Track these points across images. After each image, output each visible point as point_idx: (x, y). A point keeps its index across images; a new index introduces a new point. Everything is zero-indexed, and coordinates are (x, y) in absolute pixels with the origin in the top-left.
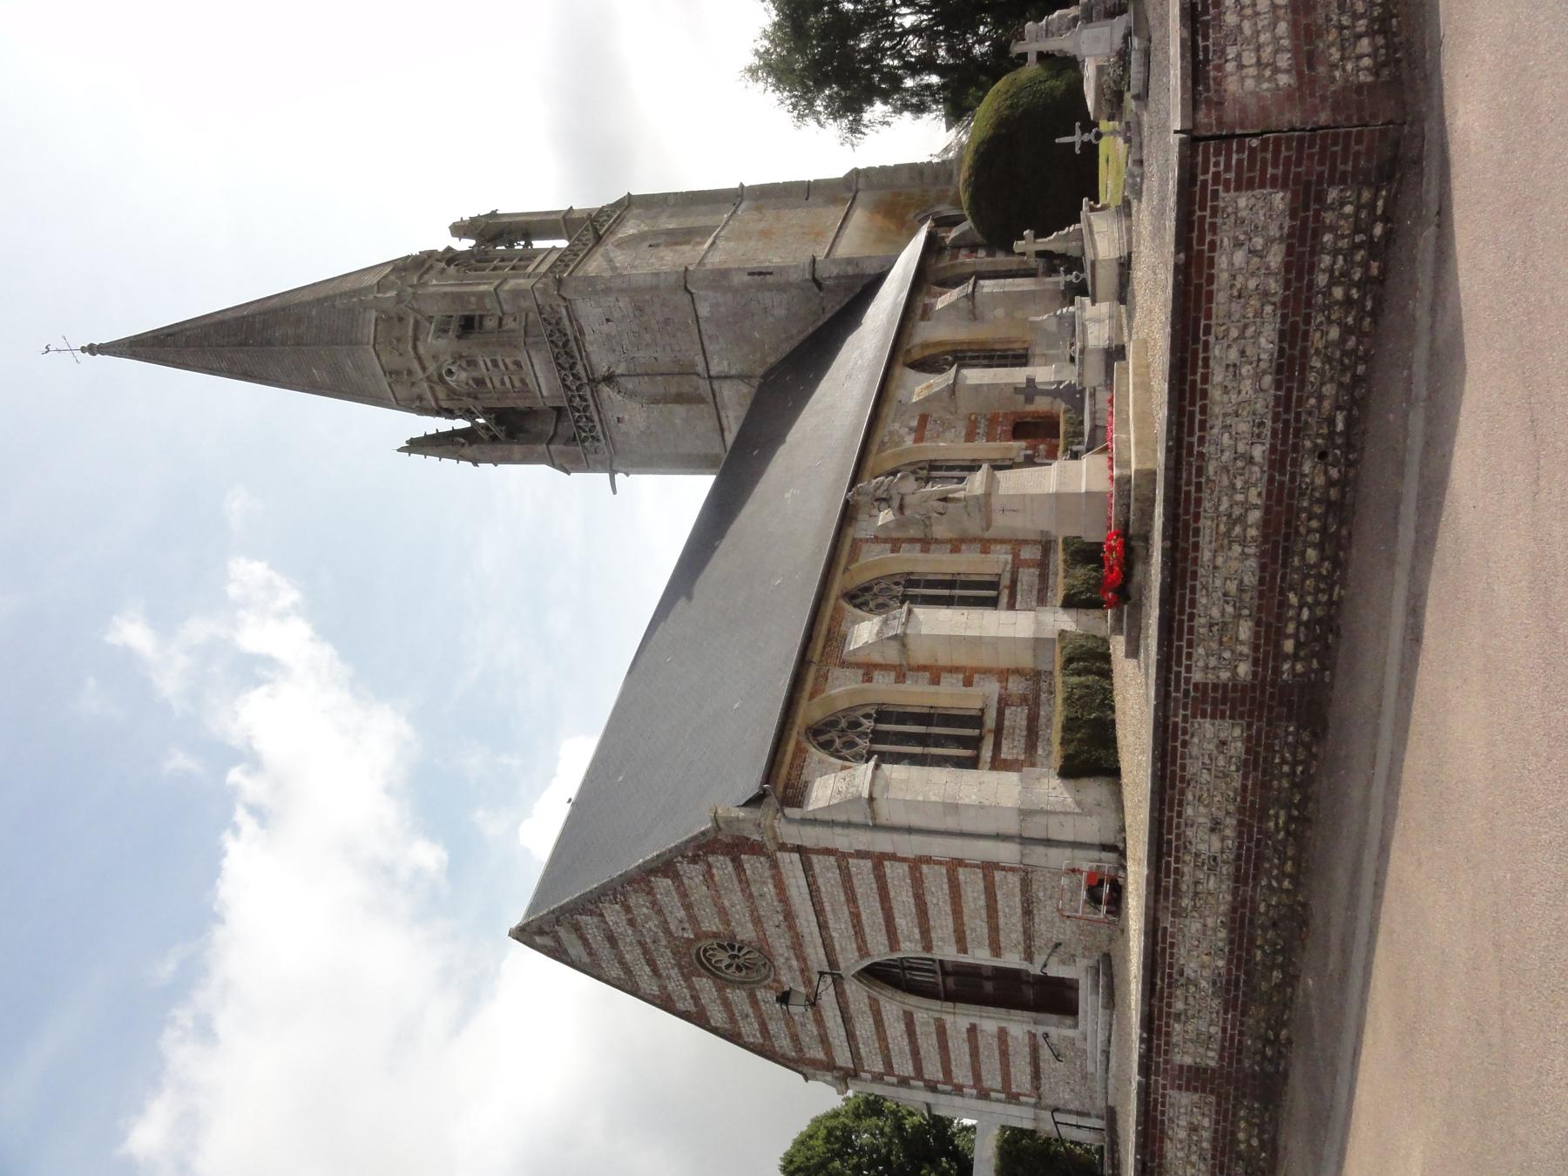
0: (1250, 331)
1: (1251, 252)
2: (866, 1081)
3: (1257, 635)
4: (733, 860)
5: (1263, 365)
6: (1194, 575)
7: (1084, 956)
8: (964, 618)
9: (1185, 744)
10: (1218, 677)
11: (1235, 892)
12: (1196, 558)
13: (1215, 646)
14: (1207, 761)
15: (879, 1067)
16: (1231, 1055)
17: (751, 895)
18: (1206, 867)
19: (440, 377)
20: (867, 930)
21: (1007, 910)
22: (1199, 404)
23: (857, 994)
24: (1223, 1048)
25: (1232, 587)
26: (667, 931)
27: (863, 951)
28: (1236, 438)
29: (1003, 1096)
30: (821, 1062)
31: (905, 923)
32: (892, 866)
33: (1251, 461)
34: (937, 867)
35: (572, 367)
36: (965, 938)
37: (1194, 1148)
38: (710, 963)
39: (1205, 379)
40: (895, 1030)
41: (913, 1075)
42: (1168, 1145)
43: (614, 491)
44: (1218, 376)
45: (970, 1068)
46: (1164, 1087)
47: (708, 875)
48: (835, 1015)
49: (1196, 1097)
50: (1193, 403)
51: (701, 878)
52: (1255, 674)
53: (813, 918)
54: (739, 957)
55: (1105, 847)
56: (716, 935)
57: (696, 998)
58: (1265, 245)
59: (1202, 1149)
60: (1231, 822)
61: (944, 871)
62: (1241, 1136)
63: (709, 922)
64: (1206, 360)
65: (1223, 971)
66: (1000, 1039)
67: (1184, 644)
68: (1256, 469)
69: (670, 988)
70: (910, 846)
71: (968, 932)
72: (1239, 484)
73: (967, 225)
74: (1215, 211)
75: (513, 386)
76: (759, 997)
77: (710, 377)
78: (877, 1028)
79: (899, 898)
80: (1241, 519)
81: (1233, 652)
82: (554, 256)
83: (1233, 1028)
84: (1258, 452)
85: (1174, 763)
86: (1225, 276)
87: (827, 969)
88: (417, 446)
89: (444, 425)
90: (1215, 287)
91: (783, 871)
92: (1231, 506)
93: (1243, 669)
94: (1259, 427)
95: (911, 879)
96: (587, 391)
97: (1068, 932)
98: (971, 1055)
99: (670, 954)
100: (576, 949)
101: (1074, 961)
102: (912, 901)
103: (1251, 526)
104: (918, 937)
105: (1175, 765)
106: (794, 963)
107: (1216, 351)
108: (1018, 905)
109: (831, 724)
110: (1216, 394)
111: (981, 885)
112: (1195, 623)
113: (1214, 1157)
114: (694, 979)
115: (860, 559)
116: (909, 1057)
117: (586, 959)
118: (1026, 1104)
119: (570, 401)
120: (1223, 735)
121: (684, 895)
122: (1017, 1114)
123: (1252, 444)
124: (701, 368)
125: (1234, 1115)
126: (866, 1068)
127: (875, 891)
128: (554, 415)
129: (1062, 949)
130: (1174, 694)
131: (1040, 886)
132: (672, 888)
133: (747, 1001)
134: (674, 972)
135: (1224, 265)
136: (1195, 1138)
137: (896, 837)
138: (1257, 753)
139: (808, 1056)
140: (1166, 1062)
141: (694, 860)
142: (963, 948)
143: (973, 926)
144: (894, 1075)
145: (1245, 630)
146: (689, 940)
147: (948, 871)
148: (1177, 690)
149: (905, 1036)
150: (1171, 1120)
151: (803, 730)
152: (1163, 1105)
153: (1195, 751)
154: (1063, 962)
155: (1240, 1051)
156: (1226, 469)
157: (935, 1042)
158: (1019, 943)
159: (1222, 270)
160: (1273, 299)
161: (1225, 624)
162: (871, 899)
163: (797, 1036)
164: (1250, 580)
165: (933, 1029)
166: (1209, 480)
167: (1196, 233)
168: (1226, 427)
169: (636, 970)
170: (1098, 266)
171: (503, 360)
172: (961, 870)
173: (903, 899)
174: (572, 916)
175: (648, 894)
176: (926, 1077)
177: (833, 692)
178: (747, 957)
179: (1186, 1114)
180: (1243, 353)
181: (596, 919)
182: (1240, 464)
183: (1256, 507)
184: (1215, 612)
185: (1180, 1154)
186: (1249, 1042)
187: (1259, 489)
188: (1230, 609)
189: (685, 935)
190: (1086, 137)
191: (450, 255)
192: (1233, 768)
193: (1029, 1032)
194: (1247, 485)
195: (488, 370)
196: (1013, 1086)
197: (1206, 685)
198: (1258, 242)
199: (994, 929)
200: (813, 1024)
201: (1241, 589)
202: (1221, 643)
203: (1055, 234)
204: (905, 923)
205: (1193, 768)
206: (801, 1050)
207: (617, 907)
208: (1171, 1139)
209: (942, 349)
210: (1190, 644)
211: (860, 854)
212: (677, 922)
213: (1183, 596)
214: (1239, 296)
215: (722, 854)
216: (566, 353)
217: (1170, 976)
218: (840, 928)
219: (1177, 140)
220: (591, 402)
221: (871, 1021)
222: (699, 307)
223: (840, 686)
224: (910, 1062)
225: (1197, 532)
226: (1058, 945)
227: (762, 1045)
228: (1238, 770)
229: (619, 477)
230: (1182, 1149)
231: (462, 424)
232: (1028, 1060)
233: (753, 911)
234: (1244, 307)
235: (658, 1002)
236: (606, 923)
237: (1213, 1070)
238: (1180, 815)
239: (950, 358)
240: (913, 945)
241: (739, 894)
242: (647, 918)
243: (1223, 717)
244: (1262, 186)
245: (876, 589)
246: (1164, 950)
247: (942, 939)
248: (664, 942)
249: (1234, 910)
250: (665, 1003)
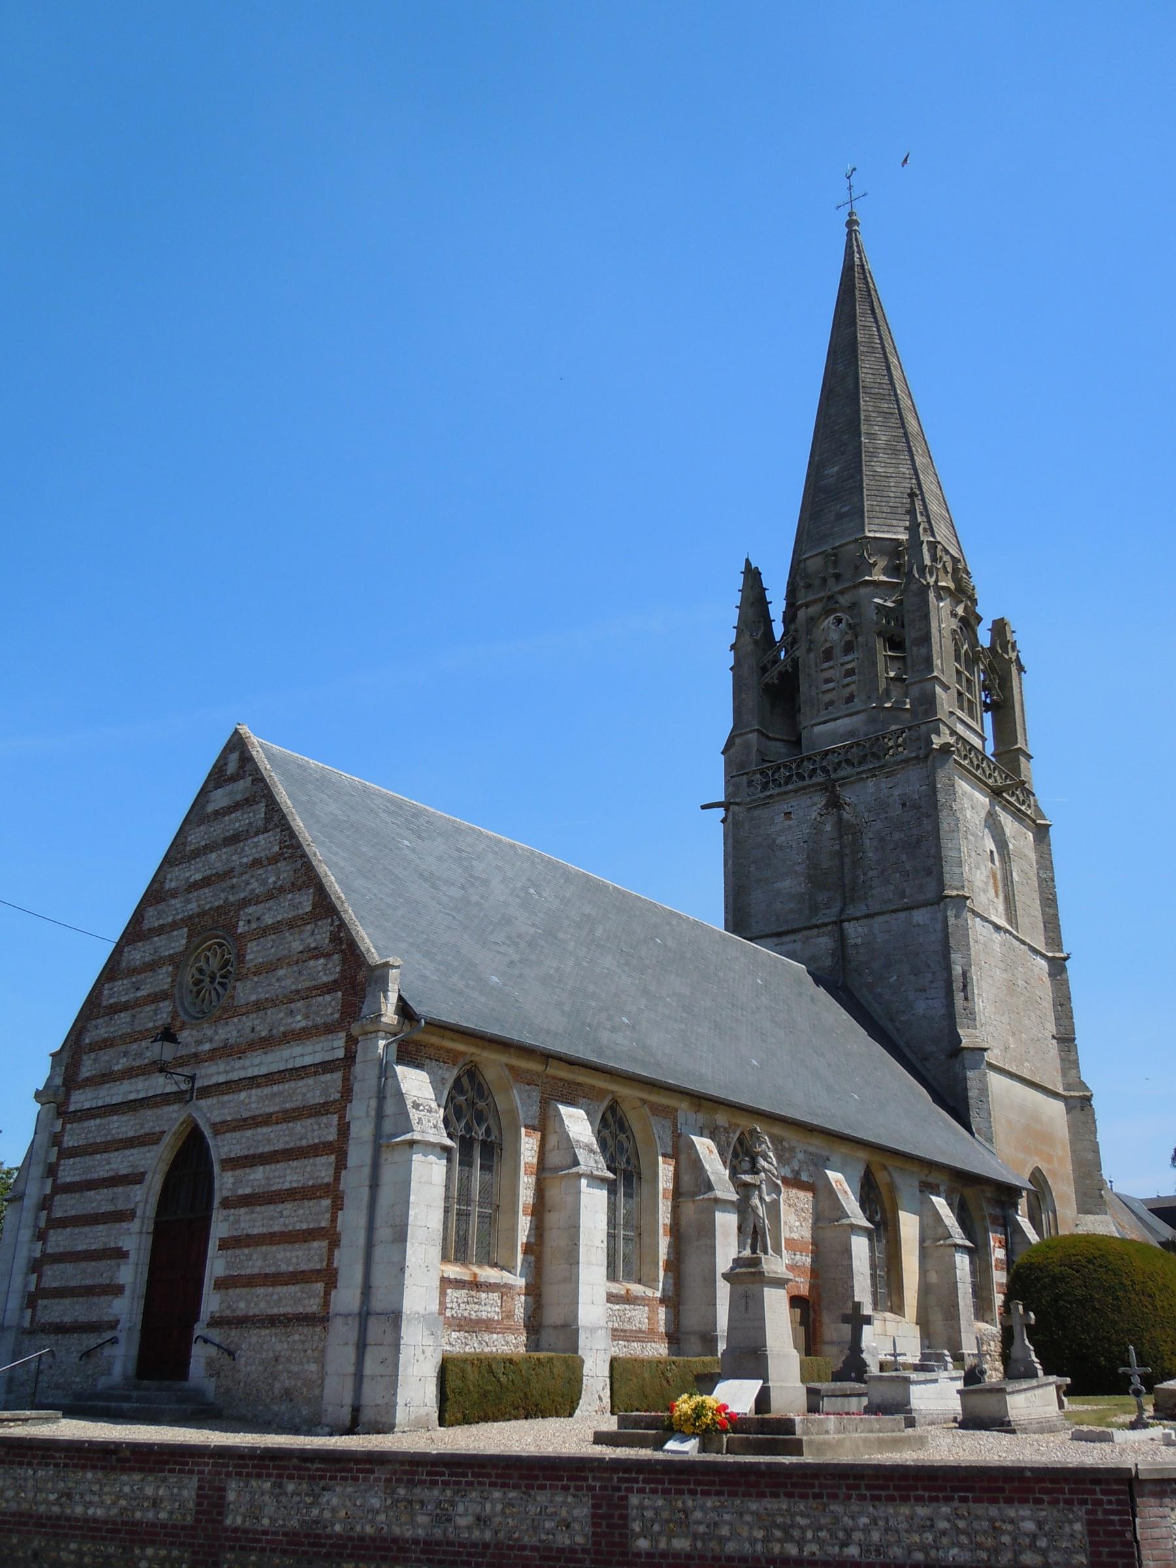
0: (964, 1540)
1: (1034, 1537)
2: (52, 1125)
3: (676, 1555)
4: (335, 981)
5: (933, 1553)
6: (733, 1494)
7: (217, 1387)
8: (598, 1243)
9: (566, 1488)
10: (634, 1520)
11: (416, 1542)
12: (750, 1495)
13: (665, 1515)
14: (550, 1510)
15: (69, 1142)
16: (238, 1539)
17: (292, 1001)
18: (438, 1511)
19: (834, 611)
20: (249, 1133)
21: (275, 1297)
22: (896, 1494)
23: (172, 1118)
24: (245, 1531)
25: (725, 1531)
26: (245, 903)
27: (220, 1128)
28: (866, 1530)
29: (32, 1288)
30: (77, 1073)
31: (257, 1178)
32: (330, 1164)
33: (844, 1545)
34: (328, 1216)
35: (849, 762)
36: (240, 1247)
37: (134, 1503)
38: (204, 950)
39: (919, 1499)
40: (120, 1162)
41: (60, 1181)
42: (137, 1477)
43: (704, 807)
44: (922, 1511)
45: (68, 1249)
46: (201, 1472)
47: (315, 953)
48: (138, 1091)
49: (191, 1505)
50: (896, 1488)
51: (313, 945)
52: (638, 1555)
53: (264, 1070)
54: (212, 982)
55: (356, 1409)
56: (241, 957)
57: (160, 930)
58: (1041, 1549)
59: (133, 1511)
60: (488, 1535)
61: (323, 1224)
62: (150, 1551)
63: (259, 951)
64: (935, 1499)
65: (329, 1530)
66: (108, 1286)
67: (666, 1485)
68: (837, 1549)
69: (173, 902)
70: (355, 1182)
71: (246, 1251)
72: (822, 1534)
73: (1033, 1237)
74: (1068, 1502)
75: (824, 692)
76: (161, 1005)
77: (842, 921)
78: (121, 1140)
79: (288, 1171)
80: (788, 1538)
81: (660, 1533)
82: (976, 742)
83: (268, 1541)
84: (853, 1551)
85: (546, 1478)
86: (1011, 1513)
87: (198, 1084)
88: (752, 576)
89: (777, 609)
90: (1002, 1505)
91: (322, 1038)
92: (801, 1527)
93: (643, 1544)
94: (876, 1550)
95: (313, 1186)
96: (820, 778)
97: (249, 1368)
98: (86, 1251)
99: (217, 904)
100: (220, 798)
101: (211, 1376)
102: (287, 1186)
103: (782, 1547)
104: (240, 1192)
105: (544, 1480)
106: (207, 1047)
107: (945, 1510)
108: (282, 1310)
109: (481, 1090)
110: (905, 1510)
111: (304, 1267)
112: (687, 1496)
113: (124, 1523)
114: (186, 930)
115: (656, 1117)
116: (84, 1177)
117: (210, 808)
118: (22, 1317)
119: (809, 759)
120: (576, 1526)
121: (291, 925)
122: (10, 1305)
123: (860, 1545)
124: (851, 911)
125: (172, 1544)
126: (69, 1126)
127: (298, 1144)
128: (793, 739)
129: (226, 1360)
130: (615, 1477)
131: (306, 1336)
132: (301, 912)
133: (157, 989)
134: (193, 907)
135: (1022, 1513)
136: (146, 1504)
137: (367, 1171)
138: (558, 1559)
139: (85, 1057)
140: (229, 1475)
141: (335, 939)
142: (224, 1245)
143: (255, 1257)
144: (59, 1159)
145: (681, 1544)
146: (236, 926)
147: (323, 1228)
148: (620, 1480)
149: (111, 1174)
150: (164, 1480)
151: (474, 1058)
152: (181, 1471)
153: (559, 1499)
154: (210, 1363)
155: (243, 1548)
156: (836, 1520)
157: (103, 1209)
158: (234, 1310)
159: (1017, 1511)
160: (993, 1558)
161: (688, 1527)
162: (287, 1139)
163: (112, 1046)
164: (731, 1547)
165: (121, 1206)
166: (825, 1506)
167: (1050, 1486)
168: (874, 1521)
169: (199, 862)
170: (999, 1396)
171: (854, 683)
172: (325, 1243)
173: (290, 1176)
174: (264, 796)
175: (293, 884)
176: (57, 1198)
177: (515, 1091)
178: (213, 992)
179: (172, 1494)
180: (944, 1533)
181: (261, 823)
182: (841, 1535)
183: (801, 1550)
184: (698, 1515)
185: (127, 1489)
186: (253, 1558)
187: (817, 1553)
188: (702, 1529)
189: (241, 923)
190: (1136, 1380)
191: (973, 621)
192: (543, 1537)
193: (118, 1322)
194: (821, 1542)
195: (842, 665)
196: (45, 1302)
197: (626, 1507)
198: (1042, 1543)
199: (251, 1281)
200: (127, 1065)
201: (722, 1540)
202: (668, 1521)
203: (1032, 1348)
204: (257, 1178)
205: (542, 1497)
206: (92, 1050)
207: (276, 848)
208: (143, 1480)
209: (887, 1205)
210: (666, 1492)
211: (344, 1130)
212: (257, 914)
213: (712, 1483)
214: (994, 1528)
215: (342, 971)
216: (865, 756)
217: (322, 1478)
218: (251, 1102)
219: (1129, 1466)
220: (807, 782)
221: (131, 1134)
222: (923, 911)
223: (521, 1099)
224: (77, 1179)
225: (775, 1495)
226: (231, 1354)
227: (99, 1005)
228: (540, 1541)
229: (720, 813)
230: (133, 1491)
231: (778, 630)
232: (81, 1319)
233: (274, 1002)
234: (985, 1532)
235: (155, 886)
236: (257, 834)
237: (221, 1522)
238: (492, 1484)
239: (878, 1218)
240: (229, 1186)
241: (293, 987)
242: (264, 882)
243: (594, 1525)
244: (1092, 1543)
245: (622, 1137)
246: (351, 1470)
247: (237, 1221)
248: (231, 898)
249: (395, 1540)
250: (155, 895)
